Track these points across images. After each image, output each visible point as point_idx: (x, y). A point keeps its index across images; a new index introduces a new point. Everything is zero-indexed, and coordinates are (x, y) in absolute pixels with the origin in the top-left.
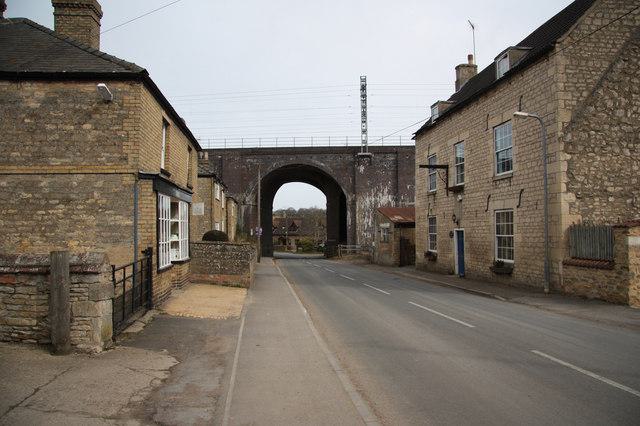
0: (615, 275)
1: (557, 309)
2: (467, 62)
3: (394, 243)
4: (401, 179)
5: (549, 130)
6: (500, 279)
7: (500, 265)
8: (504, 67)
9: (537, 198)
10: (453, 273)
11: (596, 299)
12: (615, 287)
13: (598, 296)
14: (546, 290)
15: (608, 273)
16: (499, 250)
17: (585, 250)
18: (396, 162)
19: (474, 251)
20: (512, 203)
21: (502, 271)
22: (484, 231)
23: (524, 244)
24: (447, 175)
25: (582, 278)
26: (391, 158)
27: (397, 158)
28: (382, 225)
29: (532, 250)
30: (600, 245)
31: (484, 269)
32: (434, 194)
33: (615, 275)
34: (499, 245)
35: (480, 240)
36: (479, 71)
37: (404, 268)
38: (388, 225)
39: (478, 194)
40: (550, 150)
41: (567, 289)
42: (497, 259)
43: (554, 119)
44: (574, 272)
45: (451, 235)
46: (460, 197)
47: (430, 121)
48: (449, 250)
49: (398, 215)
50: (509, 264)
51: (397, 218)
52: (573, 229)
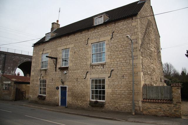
0: (173, 105)
1: (149, 122)
2: (56, 22)
3: (13, 89)
4: (6, 65)
5: (134, 46)
6: (94, 109)
7: (41, 96)
8: (101, 21)
9: (124, 74)
10: (58, 105)
11: (163, 116)
12: (173, 111)
13: (163, 115)
14: (134, 114)
15: (169, 105)
16: (92, 95)
17: (153, 95)
18: (5, 58)
19: (75, 96)
20: (105, 76)
21: (41, 98)
22: (88, 88)
23: (113, 93)
24: (56, 62)
25: (153, 108)
26: (3, 56)
27: (6, 56)
28: (4, 82)
29: (119, 96)
30: (161, 93)
31: (85, 104)
32: (46, 70)
33: (173, 105)
34: (92, 93)
35: (80, 91)
36: (60, 27)
37: (16, 102)
38: (9, 82)
39: (78, 71)
40: (134, 54)
41: (144, 112)
42: (39, 94)
43: (137, 42)
44: (148, 105)
45: (58, 88)
46: (65, 72)
47: (44, 38)
48: (56, 95)
49: (14, 78)
50: (103, 102)
51: (14, 80)
52: (145, 86)
